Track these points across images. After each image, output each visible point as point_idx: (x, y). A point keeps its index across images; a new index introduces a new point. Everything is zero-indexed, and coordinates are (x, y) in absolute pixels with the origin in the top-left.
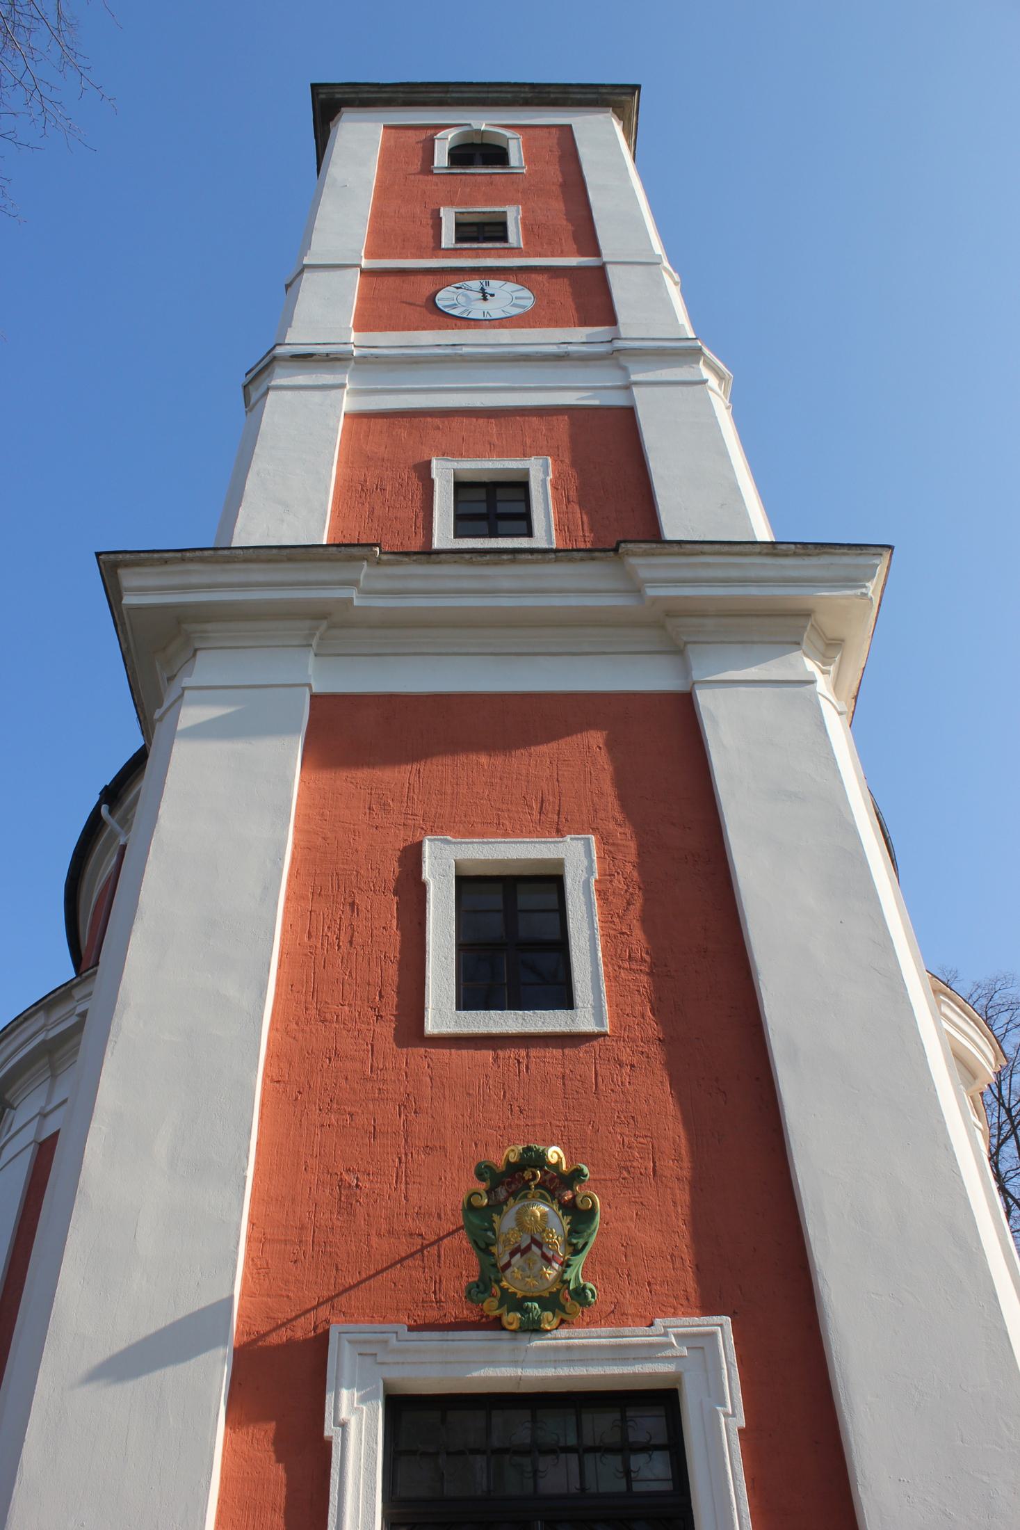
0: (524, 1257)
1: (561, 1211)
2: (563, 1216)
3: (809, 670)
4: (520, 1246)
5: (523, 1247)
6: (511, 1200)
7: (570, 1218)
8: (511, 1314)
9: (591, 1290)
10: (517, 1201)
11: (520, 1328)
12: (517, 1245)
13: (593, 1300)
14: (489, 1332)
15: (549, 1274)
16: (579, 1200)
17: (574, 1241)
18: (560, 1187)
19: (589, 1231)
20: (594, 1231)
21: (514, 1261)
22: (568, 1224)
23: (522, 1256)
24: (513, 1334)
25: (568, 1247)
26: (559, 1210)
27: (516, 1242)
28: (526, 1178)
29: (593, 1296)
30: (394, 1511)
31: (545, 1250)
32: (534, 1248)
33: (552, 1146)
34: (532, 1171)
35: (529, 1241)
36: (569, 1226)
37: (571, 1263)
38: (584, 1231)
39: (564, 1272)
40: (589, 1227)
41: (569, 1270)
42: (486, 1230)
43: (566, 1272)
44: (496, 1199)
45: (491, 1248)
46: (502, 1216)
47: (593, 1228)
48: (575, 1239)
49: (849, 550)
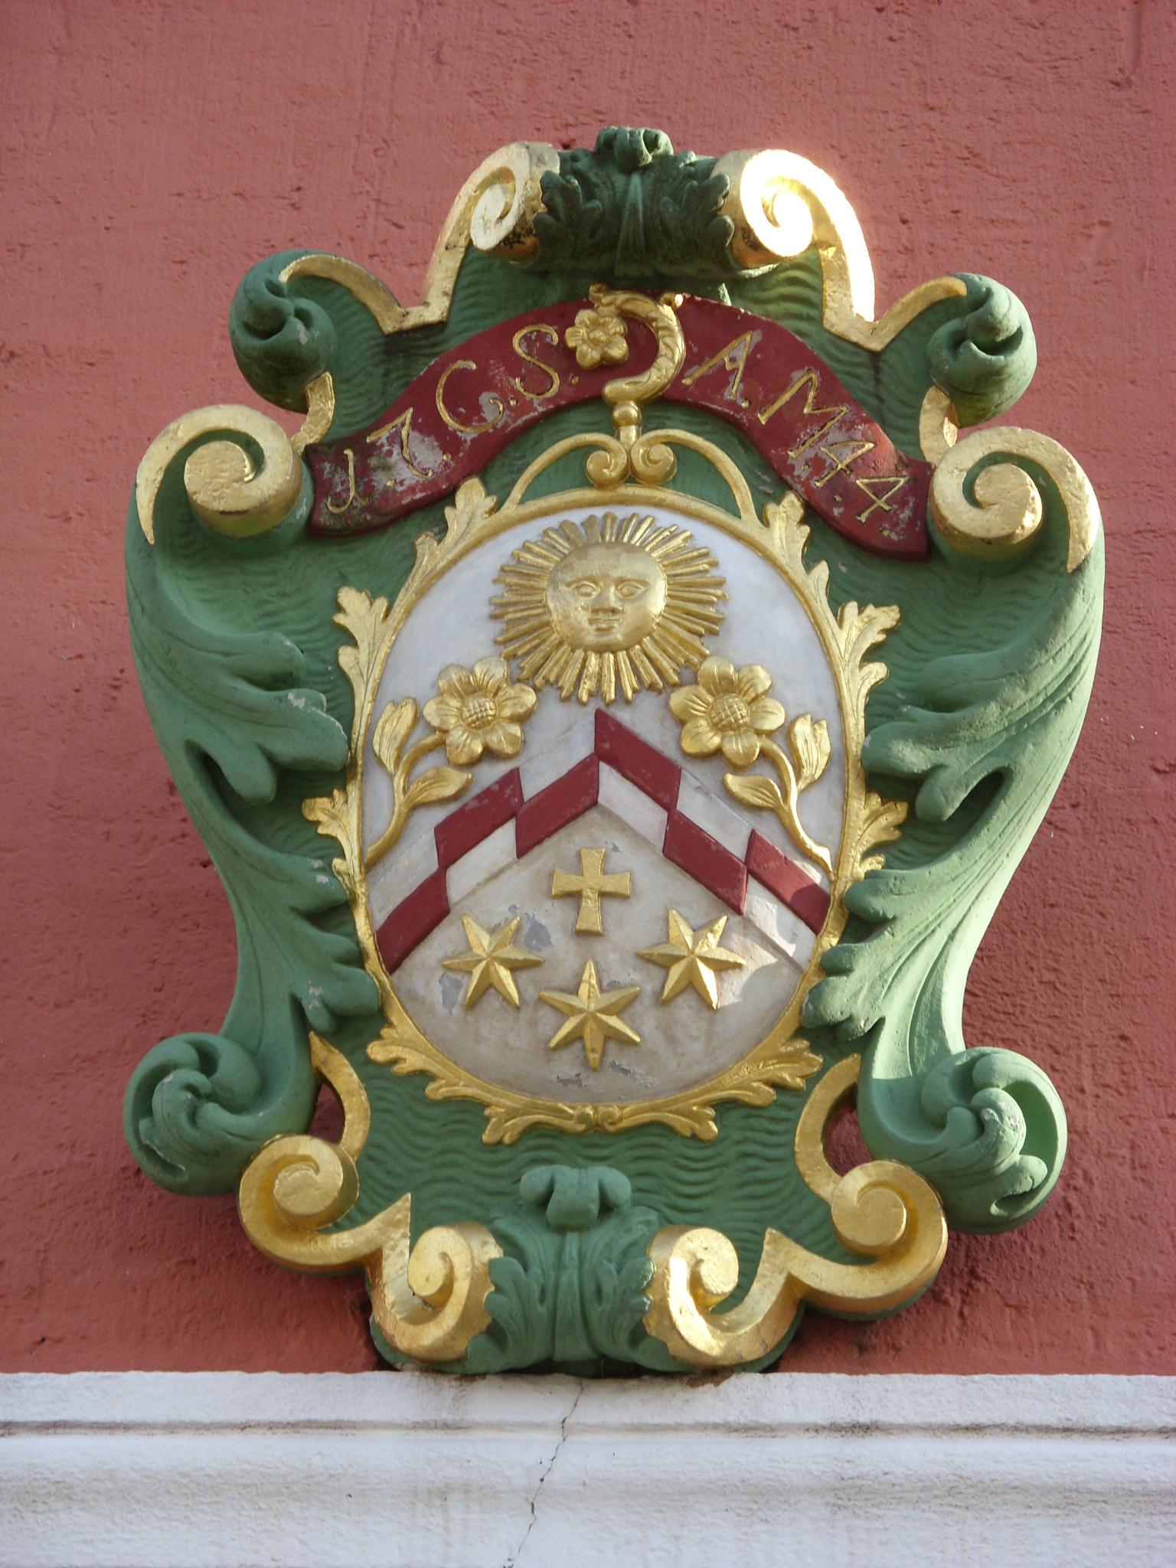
0: (545, 855)
1: (822, 571)
2: (836, 603)
3: (802, 511)
4: (512, 779)
5: (534, 785)
6: (472, 498)
7: (887, 617)
8: (440, 1239)
9: (1023, 1092)
10: (510, 508)
11: (495, 1333)
12: (491, 774)
13: (1036, 1166)
14: (270, 1379)
15: (721, 968)
16: (947, 488)
17: (912, 757)
18: (823, 420)
19: (1022, 699)
20: (1058, 699)
21: (463, 877)
22: (873, 654)
23: (524, 846)
24: (448, 1388)
25: (862, 806)
26: (809, 562)
27: (489, 754)
28: (589, 355)
29: (1040, 1140)
30: (640, 208)
31: (694, 805)
32: (613, 787)
33: (762, 146)
34: (627, 317)
35: (582, 747)
36: (878, 671)
37: (880, 905)
38: (989, 695)
39: (833, 967)
40: (1020, 670)
41: (869, 958)
42: (280, 681)
43: (844, 971)
44: (367, 490)
45: (318, 809)
46: (403, 599)
47: (1048, 675)
48: (920, 738)
49: (667, 672)
